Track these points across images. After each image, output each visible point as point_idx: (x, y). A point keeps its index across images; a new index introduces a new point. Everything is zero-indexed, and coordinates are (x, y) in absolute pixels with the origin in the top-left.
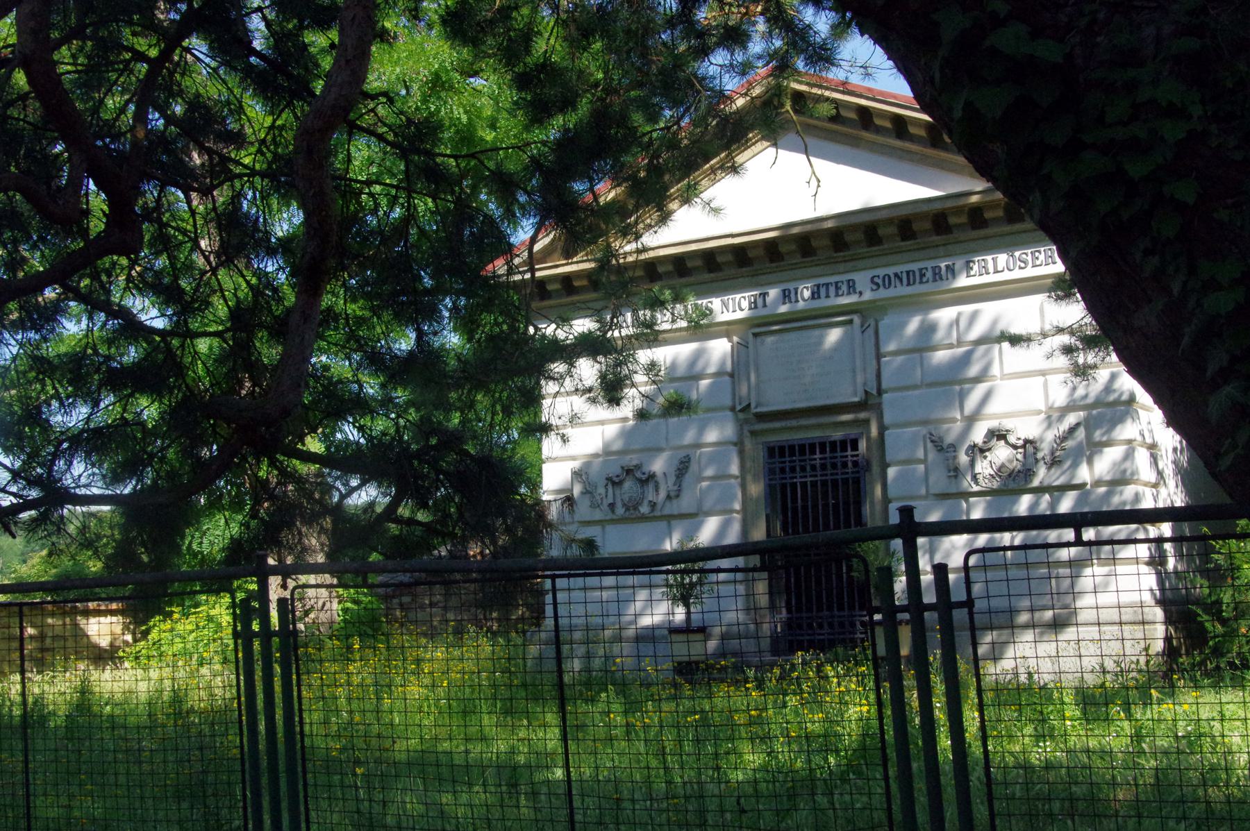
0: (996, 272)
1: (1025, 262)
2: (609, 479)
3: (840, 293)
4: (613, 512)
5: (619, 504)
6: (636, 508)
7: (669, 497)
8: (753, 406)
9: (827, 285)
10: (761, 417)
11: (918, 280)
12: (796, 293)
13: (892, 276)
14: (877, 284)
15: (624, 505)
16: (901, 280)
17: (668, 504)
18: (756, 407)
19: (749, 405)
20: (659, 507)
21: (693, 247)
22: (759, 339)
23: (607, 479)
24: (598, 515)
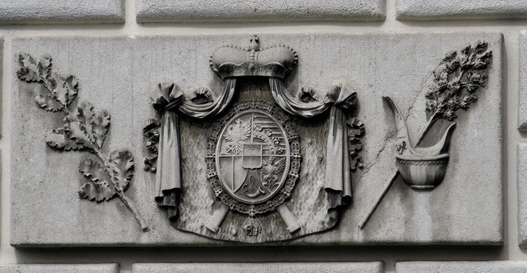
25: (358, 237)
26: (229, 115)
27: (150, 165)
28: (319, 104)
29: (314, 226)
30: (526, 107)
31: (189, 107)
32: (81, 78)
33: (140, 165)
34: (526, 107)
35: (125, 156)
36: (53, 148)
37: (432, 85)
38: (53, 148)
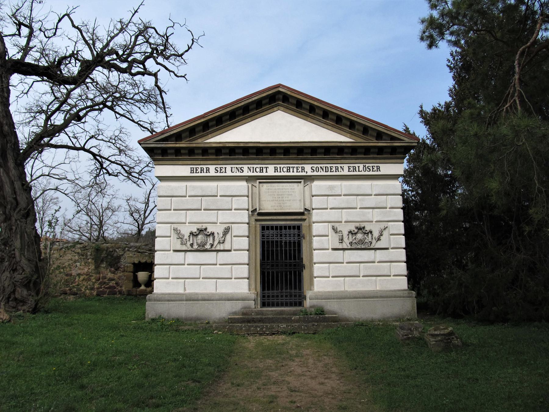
0: (359, 171)
1: (370, 169)
2: (350, 232)
3: (197, 172)
4: (192, 247)
5: (195, 244)
6: (203, 246)
7: (219, 243)
8: (258, 209)
9: (293, 167)
10: (260, 214)
11: (329, 170)
12: (280, 169)
13: (320, 168)
14: (313, 170)
15: (198, 244)
16: (323, 170)
17: (218, 246)
18: (259, 210)
19: (256, 209)
20: (214, 246)
21: (344, 144)
22: (261, 184)
23: (349, 232)
24: (184, 248)
25: (214, 249)
26: (70, 114)
27: (189, 240)
28: (209, 233)
29: (209, 248)
30: (475, 1)
31: (194, 233)
32: (181, 230)
33: (188, 240)
34: (475, 1)
35: (186, 239)
36: (177, 238)
37: (223, 231)
38: (177, 238)
